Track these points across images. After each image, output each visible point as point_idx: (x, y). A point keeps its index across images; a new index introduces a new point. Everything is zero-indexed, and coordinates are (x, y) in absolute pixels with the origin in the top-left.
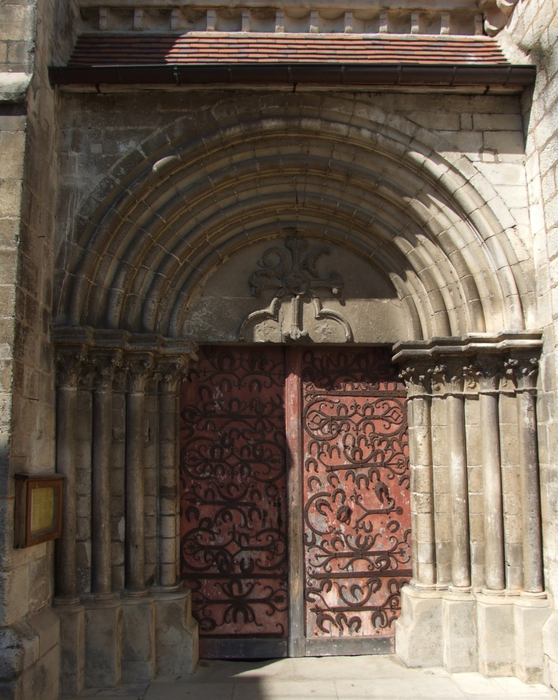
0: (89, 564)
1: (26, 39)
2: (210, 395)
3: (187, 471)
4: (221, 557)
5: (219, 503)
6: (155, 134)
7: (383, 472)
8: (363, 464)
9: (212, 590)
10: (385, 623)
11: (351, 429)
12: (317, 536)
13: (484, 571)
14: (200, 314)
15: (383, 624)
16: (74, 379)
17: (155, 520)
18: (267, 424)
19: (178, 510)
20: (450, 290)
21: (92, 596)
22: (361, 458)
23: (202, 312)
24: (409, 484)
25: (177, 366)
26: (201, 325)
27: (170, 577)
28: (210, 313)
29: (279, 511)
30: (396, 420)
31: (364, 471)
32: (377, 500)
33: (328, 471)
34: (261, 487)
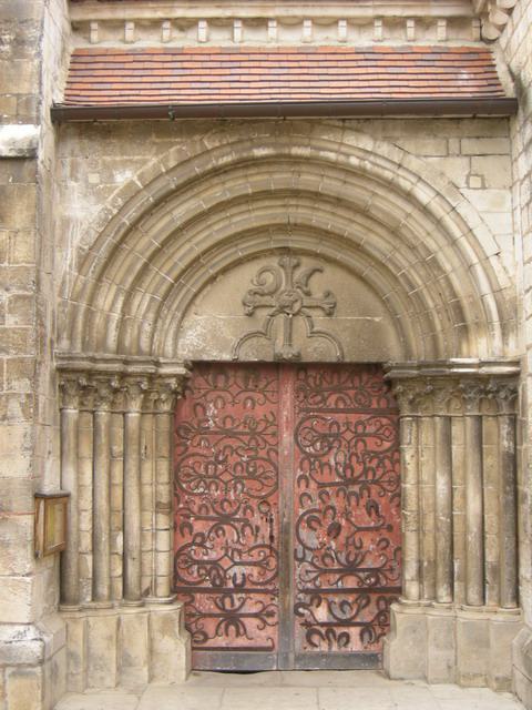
0: (90, 576)
1: (33, 92)
2: (205, 413)
3: (181, 488)
5: (213, 519)
6: (150, 164)
7: (375, 489)
8: (354, 481)
9: (205, 603)
13: (466, 589)
16: (76, 401)
17: (150, 534)
18: (260, 441)
19: (172, 524)
20: (438, 313)
21: (93, 604)
27: (163, 589)
29: (271, 527)
31: (356, 488)
32: (367, 518)
34: (254, 503)
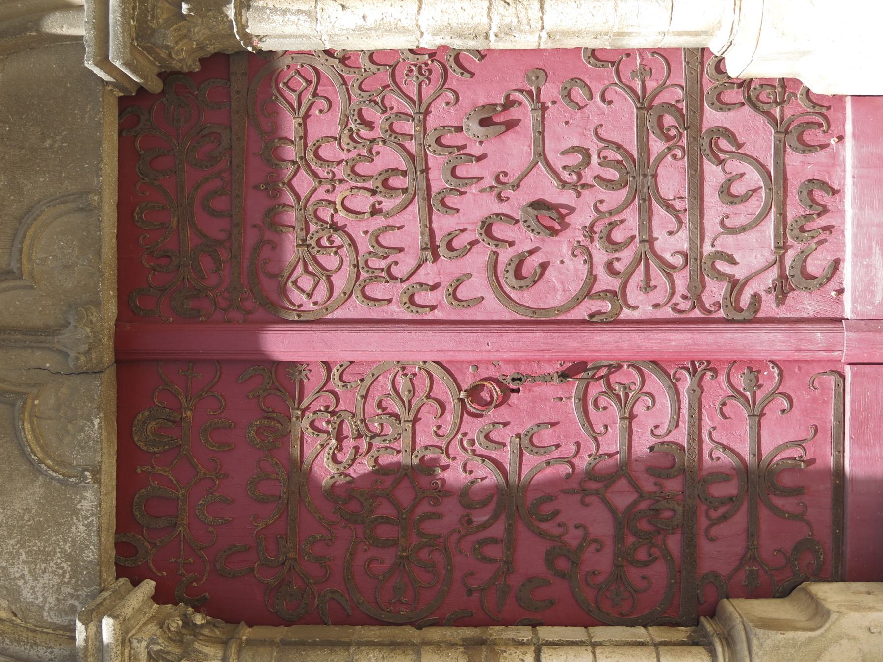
4: (644, 525)
5: (510, 529)
10: (820, 120)
11: (329, 197)
12: (597, 288)
14: (26, 582)
15: (820, 125)
22: (404, 173)
23: (22, 577)
24: (468, 50)
25: (156, 648)
26: (57, 580)
28: (23, 557)
30: (309, 82)
31: (437, 162)
33: (436, 257)
